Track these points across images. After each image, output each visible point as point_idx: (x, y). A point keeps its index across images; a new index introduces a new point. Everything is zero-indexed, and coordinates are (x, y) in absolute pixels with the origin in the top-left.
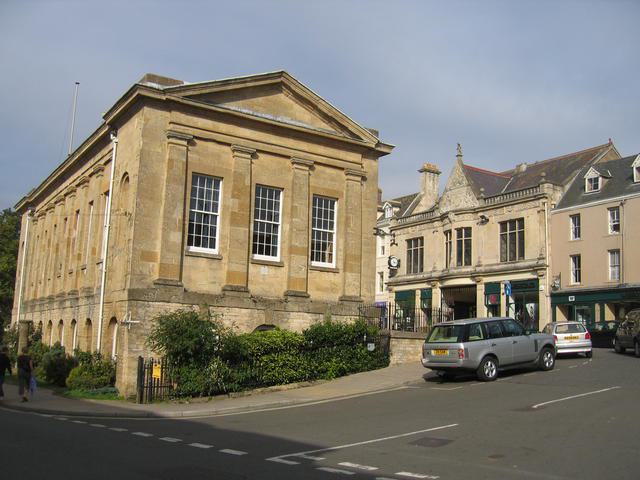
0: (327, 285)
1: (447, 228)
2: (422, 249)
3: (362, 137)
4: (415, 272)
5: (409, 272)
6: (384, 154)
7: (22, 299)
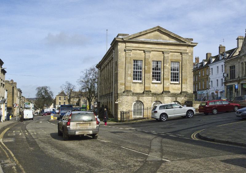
0: (176, 88)
1: (242, 61)
2: (235, 70)
3: (186, 42)
4: (233, 79)
5: (231, 78)
6: (195, 46)
7: (100, 95)
